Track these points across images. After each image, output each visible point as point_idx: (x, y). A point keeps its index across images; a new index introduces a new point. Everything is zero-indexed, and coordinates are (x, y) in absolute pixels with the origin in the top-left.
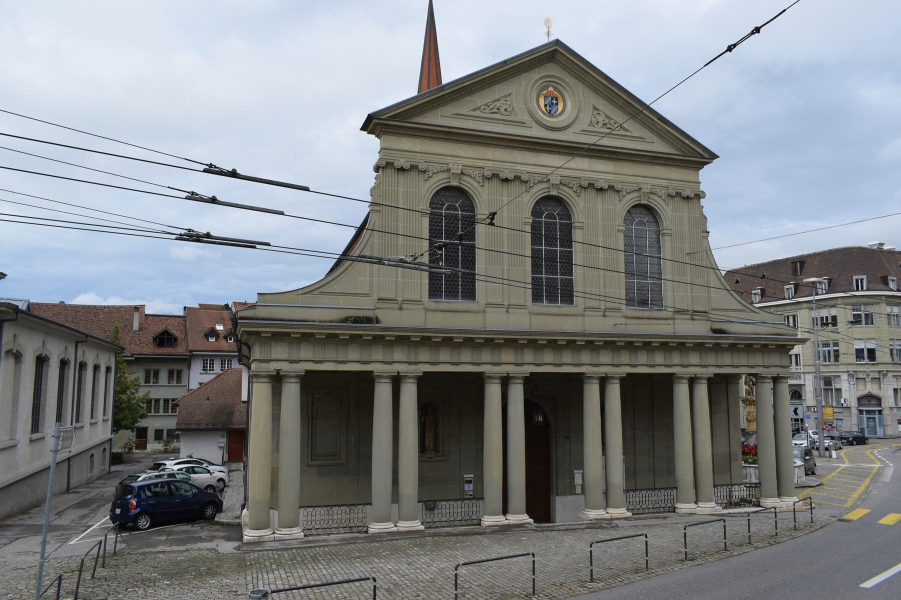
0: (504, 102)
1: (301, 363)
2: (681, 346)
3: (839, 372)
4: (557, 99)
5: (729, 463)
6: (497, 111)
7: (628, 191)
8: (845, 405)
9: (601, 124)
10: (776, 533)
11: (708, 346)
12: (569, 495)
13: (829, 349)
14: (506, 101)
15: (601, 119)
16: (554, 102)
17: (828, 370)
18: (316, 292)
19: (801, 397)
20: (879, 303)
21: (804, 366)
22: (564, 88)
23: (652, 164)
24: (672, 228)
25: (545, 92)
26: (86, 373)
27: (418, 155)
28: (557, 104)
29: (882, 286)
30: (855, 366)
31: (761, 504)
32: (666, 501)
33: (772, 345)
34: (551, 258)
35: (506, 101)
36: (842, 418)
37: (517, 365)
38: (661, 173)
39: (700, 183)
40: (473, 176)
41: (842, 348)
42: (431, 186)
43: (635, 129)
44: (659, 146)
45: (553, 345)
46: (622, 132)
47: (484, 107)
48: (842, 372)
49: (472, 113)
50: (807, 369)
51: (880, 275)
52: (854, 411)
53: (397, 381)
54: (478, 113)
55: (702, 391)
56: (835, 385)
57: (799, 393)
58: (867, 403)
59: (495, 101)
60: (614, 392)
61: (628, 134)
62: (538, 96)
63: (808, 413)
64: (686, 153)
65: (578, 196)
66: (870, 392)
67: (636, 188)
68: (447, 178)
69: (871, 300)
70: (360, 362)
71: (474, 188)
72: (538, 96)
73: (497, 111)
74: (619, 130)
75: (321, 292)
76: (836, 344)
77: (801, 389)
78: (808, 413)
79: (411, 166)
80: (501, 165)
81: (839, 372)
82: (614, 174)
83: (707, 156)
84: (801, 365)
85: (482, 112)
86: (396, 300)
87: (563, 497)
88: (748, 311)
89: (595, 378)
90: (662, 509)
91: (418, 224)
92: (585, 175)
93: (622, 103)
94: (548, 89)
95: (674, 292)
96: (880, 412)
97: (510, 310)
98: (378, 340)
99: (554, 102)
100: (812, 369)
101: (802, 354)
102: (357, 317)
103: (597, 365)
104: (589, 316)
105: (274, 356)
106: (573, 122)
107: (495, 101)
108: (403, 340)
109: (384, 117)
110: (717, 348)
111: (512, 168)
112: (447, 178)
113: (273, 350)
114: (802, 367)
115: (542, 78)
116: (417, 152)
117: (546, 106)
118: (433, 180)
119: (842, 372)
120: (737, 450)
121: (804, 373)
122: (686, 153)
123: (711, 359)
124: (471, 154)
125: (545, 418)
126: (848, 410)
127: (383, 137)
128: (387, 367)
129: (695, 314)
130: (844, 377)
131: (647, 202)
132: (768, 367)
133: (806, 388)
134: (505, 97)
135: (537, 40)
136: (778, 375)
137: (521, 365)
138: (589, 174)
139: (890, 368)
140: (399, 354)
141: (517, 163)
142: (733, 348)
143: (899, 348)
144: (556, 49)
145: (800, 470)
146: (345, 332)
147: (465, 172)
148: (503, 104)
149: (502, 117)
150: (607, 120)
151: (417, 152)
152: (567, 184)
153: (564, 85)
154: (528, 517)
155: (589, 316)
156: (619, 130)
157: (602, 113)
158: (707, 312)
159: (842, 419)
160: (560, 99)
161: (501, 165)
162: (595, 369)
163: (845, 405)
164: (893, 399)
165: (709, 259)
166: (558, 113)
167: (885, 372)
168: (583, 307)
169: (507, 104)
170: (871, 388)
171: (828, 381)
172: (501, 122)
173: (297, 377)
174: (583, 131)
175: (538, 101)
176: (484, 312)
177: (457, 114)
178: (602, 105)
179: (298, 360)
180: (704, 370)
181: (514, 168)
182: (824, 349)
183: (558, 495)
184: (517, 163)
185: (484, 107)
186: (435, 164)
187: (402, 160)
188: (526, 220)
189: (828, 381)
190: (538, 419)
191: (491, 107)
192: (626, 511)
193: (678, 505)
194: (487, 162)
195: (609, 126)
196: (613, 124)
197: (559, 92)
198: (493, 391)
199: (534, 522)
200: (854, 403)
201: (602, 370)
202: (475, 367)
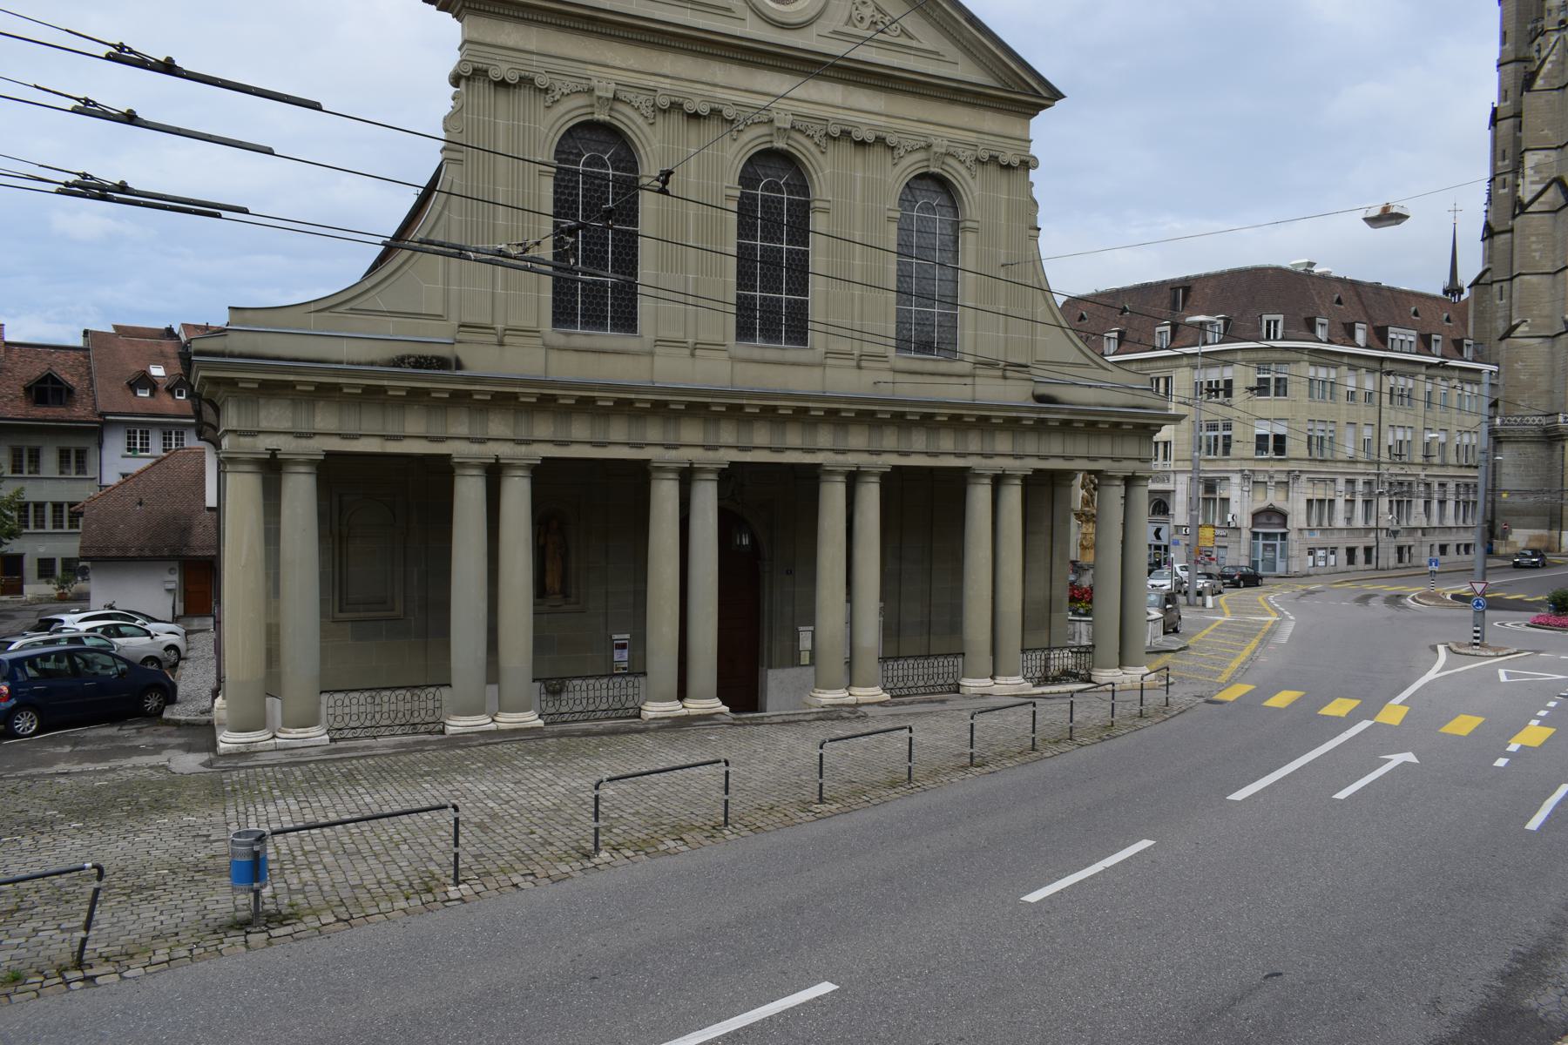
1: (317, 437)
2: (982, 422)
8: (1233, 525)
9: (867, 22)
17: (1210, 469)
18: (342, 309)
21: (1176, 460)
23: (953, 101)
27: (535, 57)
29: (1305, 333)
32: (946, 676)
33: (1127, 424)
36: (1226, 544)
41: (1237, 433)
42: (556, 122)
44: (965, 71)
46: (903, 40)
51: (1304, 315)
52: (1246, 535)
53: (494, 474)
56: (1221, 493)
60: (870, 496)
61: (914, 44)
63: (1176, 537)
64: (1010, 87)
65: (823, 153)
67: (923, 144)
74: (898, 36)
75: (352, 309)
76: (1228, 427)
77: (1168, 498)
83: (1045, 95)
87: (780, 670)
89: (840, 473)
95: (976, 330)
96: (1284, 536)
97: (698, 352)
98: (460, 400)
102: (420, 357)
105: (264, 425)
106: (819, 15)
110: (1041, 427)
111: (707, 93)
114: (1172, 462)
118: (746, 137)
121: (1175, 472)
125: (753, 539)
126: (1237, 533)
128: (475, 449)
130: (1236, 479)
138: (842, 115)
139: (1305, 466)
140: (498, 425)
146: (398, 384)
147: (621, 95)
150: (878, 16)
152: (803, 128)
156: (898, 36)
158: (1027, 367)
159: (1226, 547)
162: (840, 458)
167: (1297, 473)
168: (824, 350)
170: (1274, 498)
171: (1210, 486)
173: (310, 462)
174: (835, 32)
176: (651, 354)
180: (1017, 463)
188: (730, 192)
192: (1023, 680)
193: (965, 682)
194: (662, 79)
198: (665, 494)
199: (731, 711)
200: (1246, 522)
201: (852, 460)
202: (634, 450)
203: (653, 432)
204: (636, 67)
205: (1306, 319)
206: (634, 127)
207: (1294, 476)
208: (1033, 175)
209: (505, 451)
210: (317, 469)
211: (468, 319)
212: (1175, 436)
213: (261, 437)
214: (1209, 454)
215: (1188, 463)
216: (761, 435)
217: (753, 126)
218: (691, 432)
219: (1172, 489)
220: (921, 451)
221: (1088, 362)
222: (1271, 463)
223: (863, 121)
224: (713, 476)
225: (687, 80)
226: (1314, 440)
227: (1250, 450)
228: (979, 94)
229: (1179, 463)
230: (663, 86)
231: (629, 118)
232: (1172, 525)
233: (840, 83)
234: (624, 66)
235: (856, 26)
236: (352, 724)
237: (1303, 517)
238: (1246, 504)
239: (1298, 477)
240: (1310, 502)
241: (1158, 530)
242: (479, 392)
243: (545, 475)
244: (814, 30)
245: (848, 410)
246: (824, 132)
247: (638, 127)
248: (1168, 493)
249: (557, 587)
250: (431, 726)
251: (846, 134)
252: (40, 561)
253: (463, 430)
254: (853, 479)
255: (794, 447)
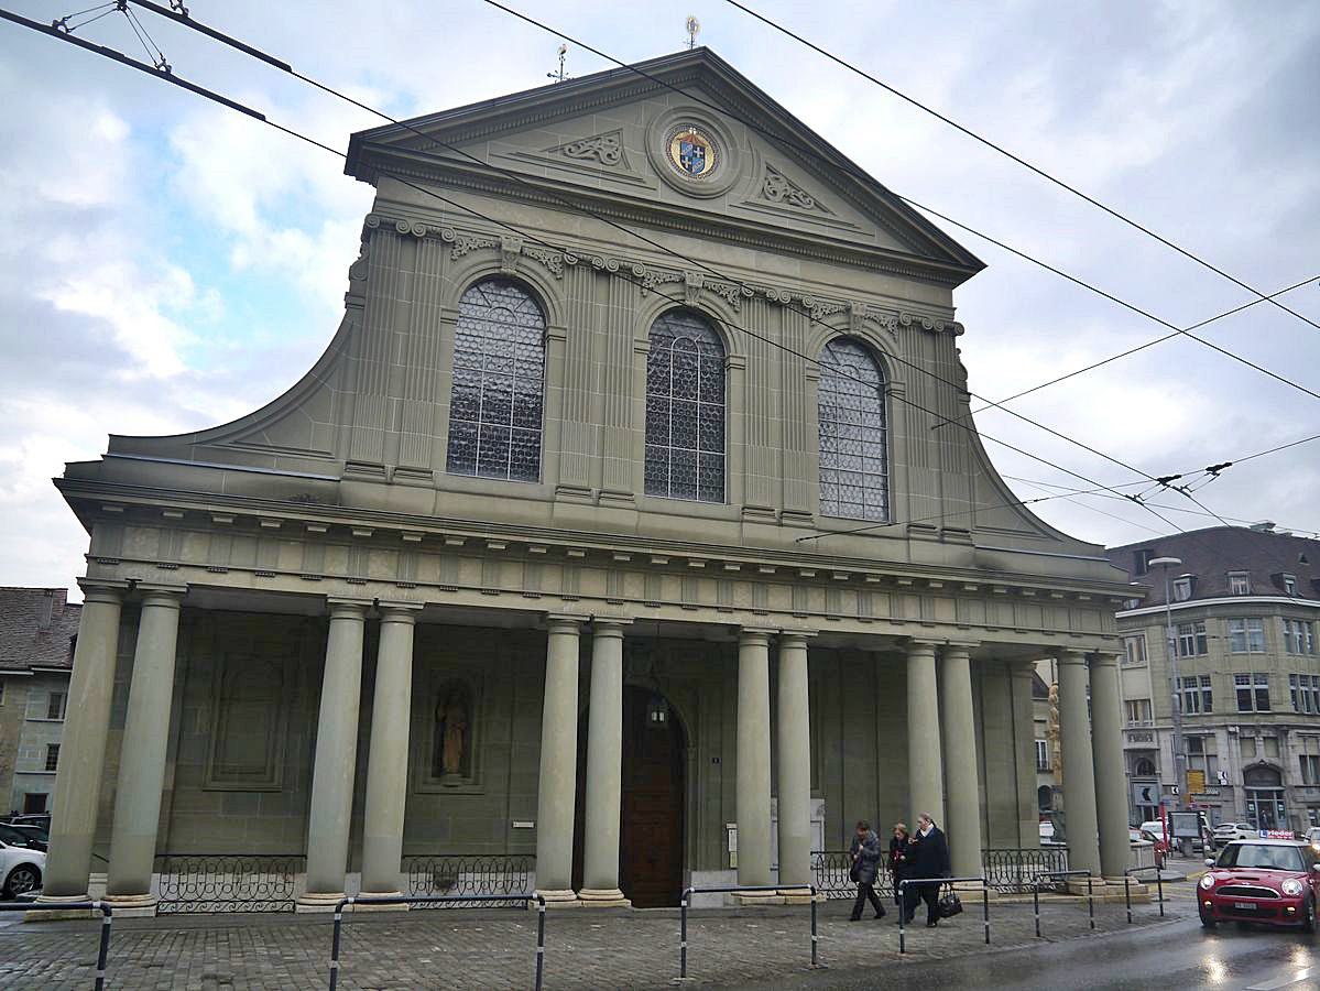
0: (608, 143)
2: (920, 587)
3: (1212, 728)
4: (702, 149)
5: (1015, 822)
6: (593, 156)
7: (827, 312)
8: (1224, 783)
9: (780, 195)
10: (1092, 923)
11: (1057, 596)
12: (715, 870)
13: (1195, 689)
14: (611, 141)
15: (780, 187)
16: (698, 152)
17: (1193, 727)
19: (1154, 769)
20: (1271, 616)
21: (1156, 719)
22: (716, 131)
23: (871, 269)
24: (905, 381)
25: (682, 135)
26: (165, 785)
27: (443, 215)
28: (703, 157)
29: (1274, 590)
30: (1237, 717)
31: (1071, 889)
33: (1084, 594)
34: (685, 416)
35: (611, 141)
36: (1219, 803)
37: (648, 604)
38: (886, 286)
39: (955, 309)
40: (544, 262)
41: (1216, 688)
43: (842, 212)
44: (880, 240)
45: (679, 568)
47: (570, 146)
48: (1217, 727)
49: (547, 155)
50: (1163, 724)
51: (1270, 572)
52: (1239, 792)
53: (374, 621)
54: (558, 156)
55: (961, 671)
56: (1208, 748)
57: (1150, 763)
58: (1258, 779)
59: (591, 139)
60: (797, 663)
61: (829, 216)
62: (669, 141)
63: (1165, 797)
65: (736, 312)
66: (1262, 761)
67: (843, 308)
68: (493, 261)
69: (1257, 611)
70: (300, 575)
71: (545, 282)
72: (669, 141)
73: (593, 156)
74: (811, 209)
76: (1206, 680)
77: (1153, 756)
78: (1165, 797)
79: (427, 232)
80: (598, 247)
81: (1212, 728)
82: (802, 280)
83: (964, 263)
84: (1153, 716)
85: (565, 154)
86: (383, 467)
87: (706, 873)
88: (1042, 535)
90: (885, 891)
91: (431, 335)
92: (748, 278)
93: (818, 164)
94: (687, 131)
95: (908, 493)
96: (1280, 794)
98: (339, 536)
99: (698, 152)
100: (1169, 724)
101: (1154, 698)
103: (764, 613)
104: (747, 521)
105: (127, 554)
106: (730, 188)
107: (591, 139)
108: (388, 538)
109: (382, 142)
110: (985, 594)
111: (617, 253)
112: (493, 261)
113: (128, 541)
114: (1153, 721)
115: (676, 110)
116: (442, 211)
117: (682, 158)
118: (468, 262)
119: (1217, 727)
120: (1030, 797)
121: (1156, 729)
122: (922, 253)
123: (975, 614)
124: (541, 222)
125: (672, 714)
126: (1228, 791)
127: (382, 180)
128: (352, 591)
129: (944, 535)
130: (1221, 735)
131: (858, 333)
132: (1078, 635)
133: (1162, 755)
134: (609, 134)
135: (662, 42)
136: (1097, 650)
137: (619, 602)
138: (756, 277)
139: (1293, 720)
140: (380, 566)
141: (626, 246)
142: (1015, 596)
143: (1304, 665)
144: (703, 64)
145: (1145, 853)
146: (272, 516)
147: (526, 251)
148: (605, 146)
149: (601, 167)
150: (791, 191)
151: (442, 211)
152: (716, 289)
153: (716, 126)
154: (623, 896)
155: (747, 521)
156: (811, 209)
157: (782, 179)
158: (967, 532)
159: (1219, 806)
160: (708, 149)
161: (598, 247)
162: (760, 620)
163: (1224, 783)
164: (1300, 773)
165: (972, 441)
166: (704, 171)
167: (1285, 728)
168: (741, 506)
169: (612, 147)
170: (1264, 754)
171: (1195, 743)
172: (600, 175)
174: (747, 203)
175: (669, 149)
177: (518, 154)
178: (783, 165)
179: (175, 564)
180: (962, 634)
181: (621, 254)
182: (1188, 690)
183: (695, 870)
184: (626, 246)
185: (570, 146)
186: (475, 235)
187: (412, 222)
188: (639, 345)
189: (1195, 743)
190: (658, 717)
191: (583, 149)
194: (570, 239)
195: (794, 200)
196: (801, 197)
197: (709, 137)
198: (564, 653)
199: (633, 905)
200: (1238, 779)
201: (775, 622)
203: (550, 581)
204: (545, 227)
205: (1272, 576)
206: (541, 282)
207: (1281, 732)
208: (959, 342)
209: (386, 594)
210: (181, 605)
211: (355, 458)
212: (1154, 693)
213: (122, 565)
214: (1185, 654)
215: (1169, 721)
216: (671, 591)
217: (664, 285)
218: (593, 584)
219: (1157, 747)
220: (852, 617)
221: (1032, 529)
222: (1257, 717)
223: (778, 284)
224: (804, 645)
225: (598, 241)
226: (1299, 696)
227: (1233, 707)
228: (898, 261)
229: (1161, 721)
230: (572, 245)
231: (538, 274)
232: (1160, 785)
233: (754, 249)
234: (533, 226)
235: (768, 199)
236: (189, 897)
237: (1298, 774)
238: (1236, 761)
239: (1286, 733)
240: (1302, 758)
241: (1147, 790)
242: (359, 528)
243: (433, 632)
244: (726, 200)
245: (768, 565)
246: (737, 293)
247: (545, 282)
248: (1152, 752)
249: (455, 765)
250: (279, 904)
251: (761, 296)
252: (43, 797)
253: (342, 571)
254: (778, 644)
255: (708, 607)
